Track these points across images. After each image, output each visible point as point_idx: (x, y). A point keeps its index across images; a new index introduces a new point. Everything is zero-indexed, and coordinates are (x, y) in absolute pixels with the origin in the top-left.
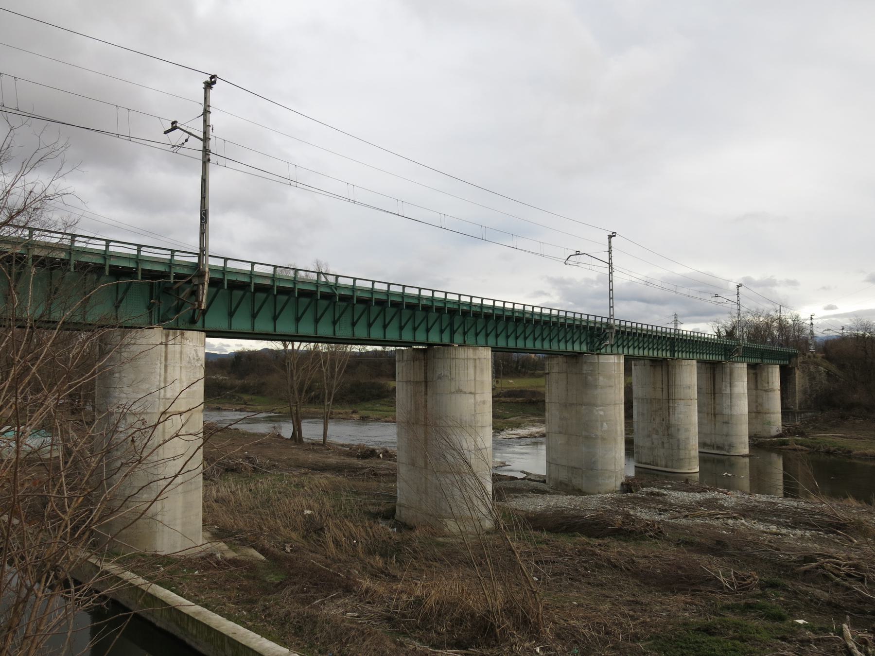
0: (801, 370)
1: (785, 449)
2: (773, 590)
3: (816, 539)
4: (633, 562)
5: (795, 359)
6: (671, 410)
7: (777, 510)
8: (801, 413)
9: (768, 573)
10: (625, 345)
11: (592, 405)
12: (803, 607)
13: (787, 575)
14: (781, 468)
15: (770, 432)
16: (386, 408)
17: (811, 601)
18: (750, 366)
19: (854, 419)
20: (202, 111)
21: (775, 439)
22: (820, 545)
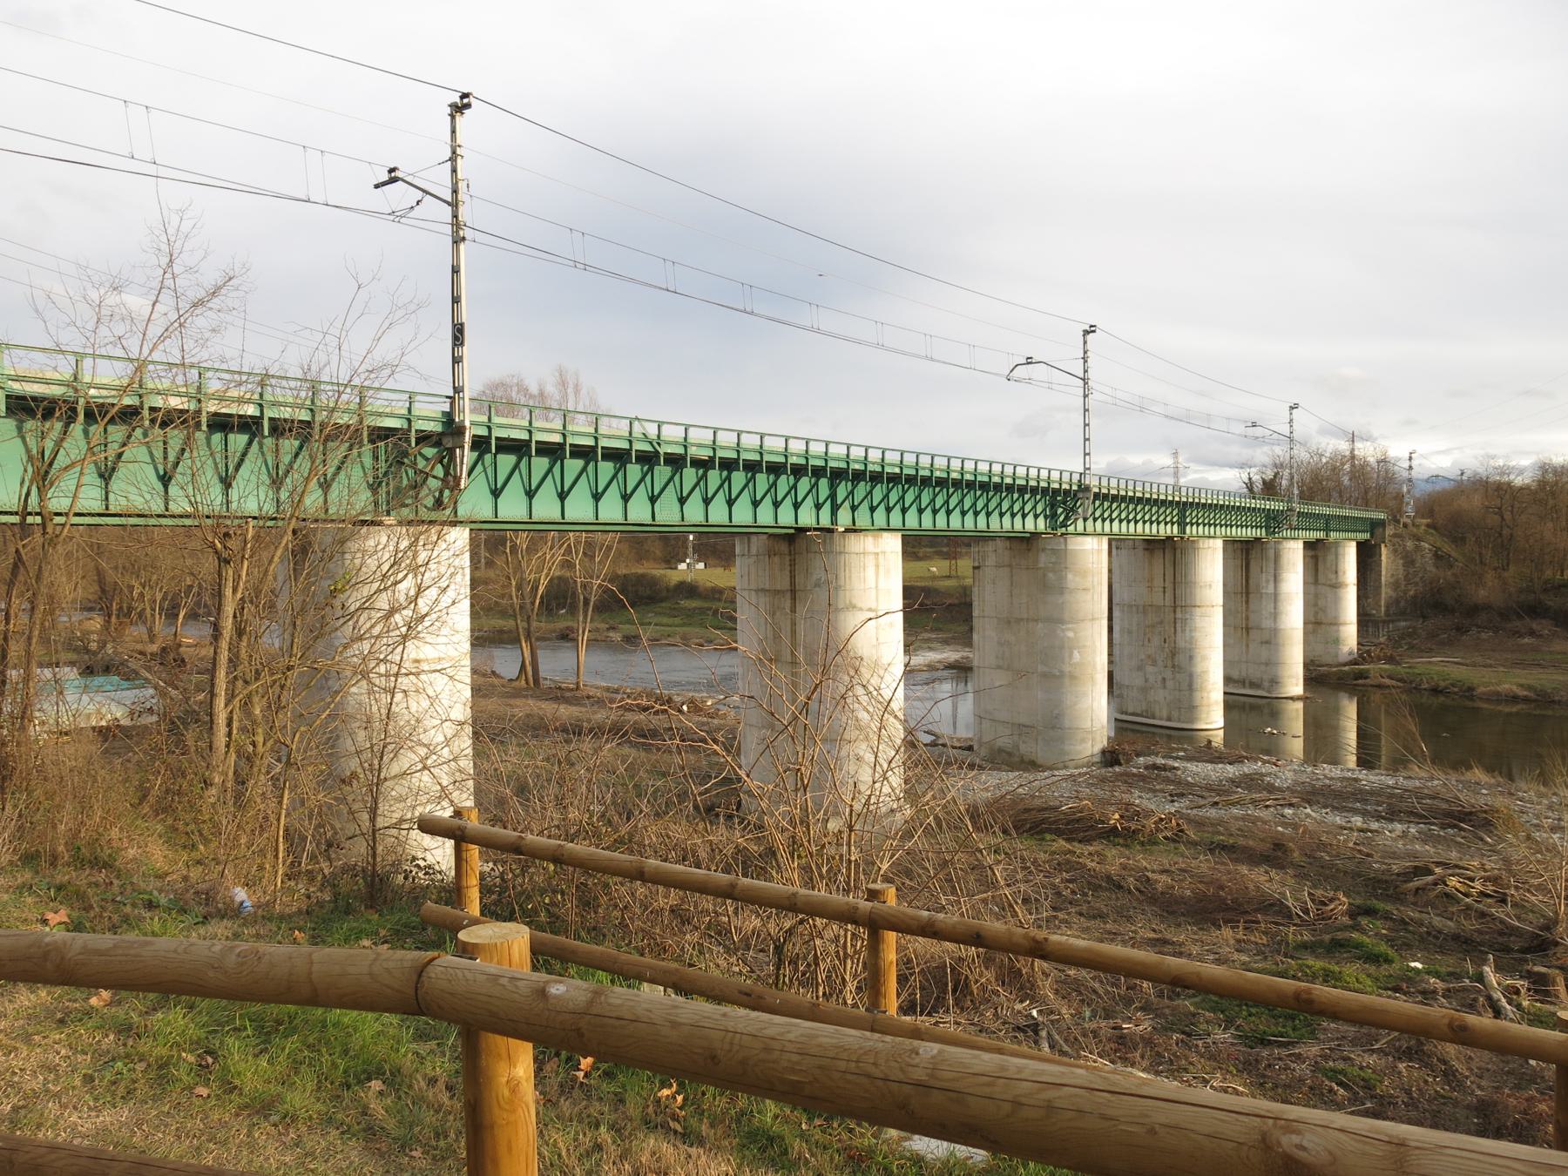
0: (1391, 548)
1: (1363, 685)
2: (1370, 919)
3: (1426, 838)
4: (1148, 879)
5: (1381, 530)
6: (1178, 625)
7: (1361, 791)
8: (1389, 621)
9: (1359, 893)
10: (1097, 516)
11: (1058, 621)
12: (1417, 943)
13: (1387, 895)
14: (1355, 717)
15: (1337, 656)
16: (665, 620)
17: (1429, 933)
18: (1309, 546)
19: (1479, 632)
20: (449, 154)
21: (1346, 668)
22: (1434, 847)
